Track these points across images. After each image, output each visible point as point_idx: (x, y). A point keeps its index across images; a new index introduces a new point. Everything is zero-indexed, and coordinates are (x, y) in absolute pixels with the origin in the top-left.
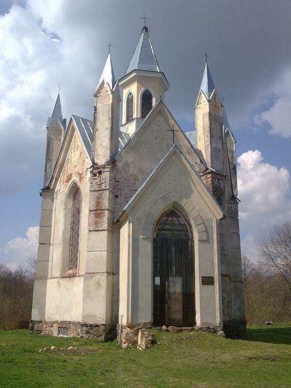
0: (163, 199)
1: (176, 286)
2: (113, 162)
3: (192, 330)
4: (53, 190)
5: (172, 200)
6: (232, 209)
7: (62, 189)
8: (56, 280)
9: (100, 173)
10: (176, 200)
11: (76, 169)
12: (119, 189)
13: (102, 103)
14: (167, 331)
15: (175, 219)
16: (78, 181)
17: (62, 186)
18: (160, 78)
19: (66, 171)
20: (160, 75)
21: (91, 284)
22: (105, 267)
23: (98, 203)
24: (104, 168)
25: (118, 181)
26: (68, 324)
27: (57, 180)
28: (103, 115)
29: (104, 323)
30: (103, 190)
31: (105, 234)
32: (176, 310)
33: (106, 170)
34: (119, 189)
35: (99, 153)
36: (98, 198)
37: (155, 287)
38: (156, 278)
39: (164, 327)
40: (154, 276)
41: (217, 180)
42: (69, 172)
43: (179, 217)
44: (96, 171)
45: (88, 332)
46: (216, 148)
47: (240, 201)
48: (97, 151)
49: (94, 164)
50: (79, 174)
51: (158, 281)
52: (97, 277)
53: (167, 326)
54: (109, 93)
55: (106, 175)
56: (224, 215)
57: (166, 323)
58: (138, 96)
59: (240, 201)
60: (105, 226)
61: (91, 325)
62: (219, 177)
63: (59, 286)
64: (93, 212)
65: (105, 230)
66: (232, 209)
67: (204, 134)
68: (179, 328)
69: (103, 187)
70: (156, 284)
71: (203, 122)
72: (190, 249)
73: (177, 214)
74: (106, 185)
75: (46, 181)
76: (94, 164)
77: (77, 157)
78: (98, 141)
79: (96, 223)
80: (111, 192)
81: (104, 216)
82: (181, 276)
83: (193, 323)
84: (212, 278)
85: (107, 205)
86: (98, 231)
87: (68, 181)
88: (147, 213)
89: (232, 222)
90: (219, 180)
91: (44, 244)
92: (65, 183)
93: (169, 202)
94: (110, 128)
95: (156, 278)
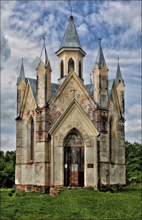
0: (69, 127)
1: (75, 168)
2: (47, 107)
3: (82, 188)
4: (22, 119)
5: (73, 127)
6: (121, 125)
7: (26, 118)
8: (25, 165)
9: (41, 112)
10: (75, 127)
11: (32, 108)
12: (51, 120)
13: (40, 74)
14: (70, 189)
15: (75, 136)
16: (32, 115)
17: (26, 117)
18: (79, 51)
19: (27, 109)
20: (78, 49)
21: (38, 167)
22: (44, 159)
23: (40, 128)
24: (42, 109)
25: (51, 116)
26: (31, 186)
27: (23, 113)
28: (41, 80)
29: (44, 185)
30: (42, 121)
31: (44, 143)
32: (75, 180)
33: (43, 110)
34: (51, 120)
35: (40, 101)
36: (40, 125)
37: (65, 169)
38: (65, 165)
39: (69, 187)
40: (65, 163)
41: (103, 113)
42: (28, 109)
43: (78, 135)
44: (38, 111)
45: (37, 189)
46: (104, 95)
47: (126, 121)
48: (39, 100)
49: (38, 107)
50: (33, 111)
51: (66, 166)
52: (40, 165)
53: (70, 187)
54: (44, 68)
55: (44, 113)
56: (99, 134)
57: (70, 185)
58: (66, 62)
59: (126, 121)
60: (44, 140)
61: (39, 186)
62: (104, 111)
63: (27, 168)
64: (38, 133)
65: (44, 142)
66: (121, 125)
67: (97, 87)
68: (76, 188)
69: (42, 120)
70: (65, 168)
71: (97, 80)
72: (82, 151)
73: (76, 134)
74: (44, 119)
75: (17, 114)
76: (38, 107)
77: (32, 101)
78: (39, 95)
79: (40, 138)
80: (46, 121)
81: (43, 134)
82: (77, 164)
83: (83, 185)
84: (93, 164)
85: (44, 129)
86: (40, 142)
87: (28, 114)
88: (60, 134)
89: (121, 132)
90: (104, 113)
91: (19, 147)
92: (27, 115)
93: (71, 128)
94: (44, 88)
95: (65, 165)
